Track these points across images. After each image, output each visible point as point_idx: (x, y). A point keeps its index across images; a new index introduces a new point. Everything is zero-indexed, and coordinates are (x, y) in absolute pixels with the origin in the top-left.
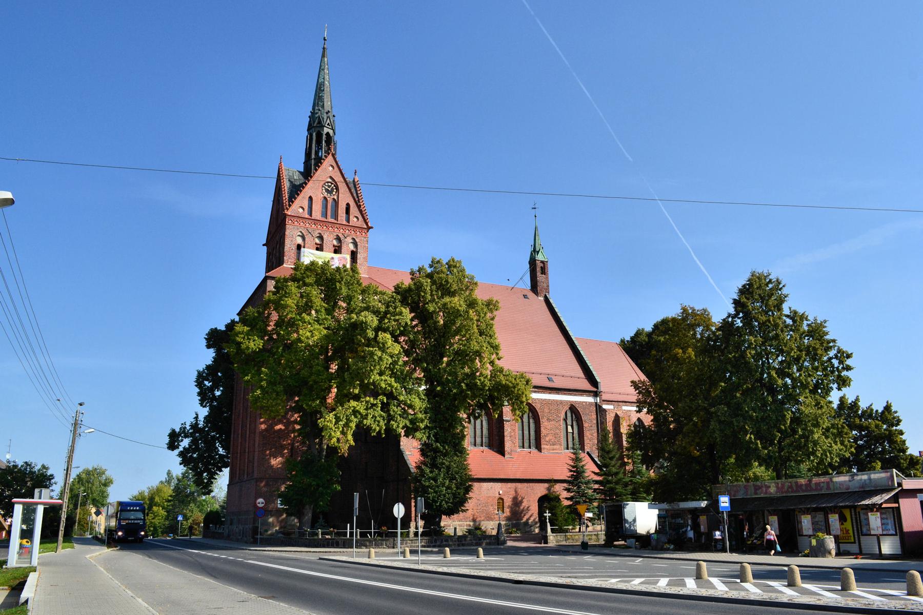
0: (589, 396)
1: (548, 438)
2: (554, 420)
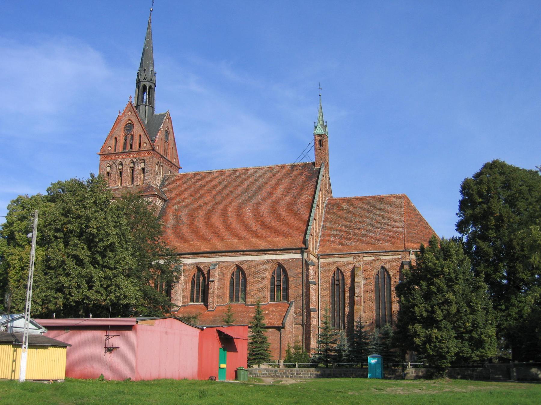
0: (297, 253)
1: (253, 293)
2: (259, 277)
